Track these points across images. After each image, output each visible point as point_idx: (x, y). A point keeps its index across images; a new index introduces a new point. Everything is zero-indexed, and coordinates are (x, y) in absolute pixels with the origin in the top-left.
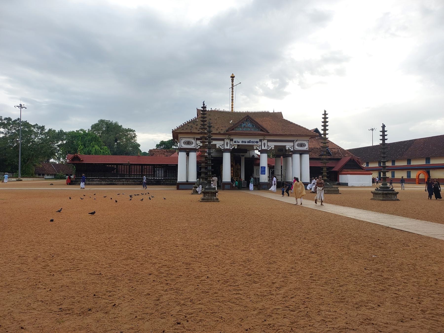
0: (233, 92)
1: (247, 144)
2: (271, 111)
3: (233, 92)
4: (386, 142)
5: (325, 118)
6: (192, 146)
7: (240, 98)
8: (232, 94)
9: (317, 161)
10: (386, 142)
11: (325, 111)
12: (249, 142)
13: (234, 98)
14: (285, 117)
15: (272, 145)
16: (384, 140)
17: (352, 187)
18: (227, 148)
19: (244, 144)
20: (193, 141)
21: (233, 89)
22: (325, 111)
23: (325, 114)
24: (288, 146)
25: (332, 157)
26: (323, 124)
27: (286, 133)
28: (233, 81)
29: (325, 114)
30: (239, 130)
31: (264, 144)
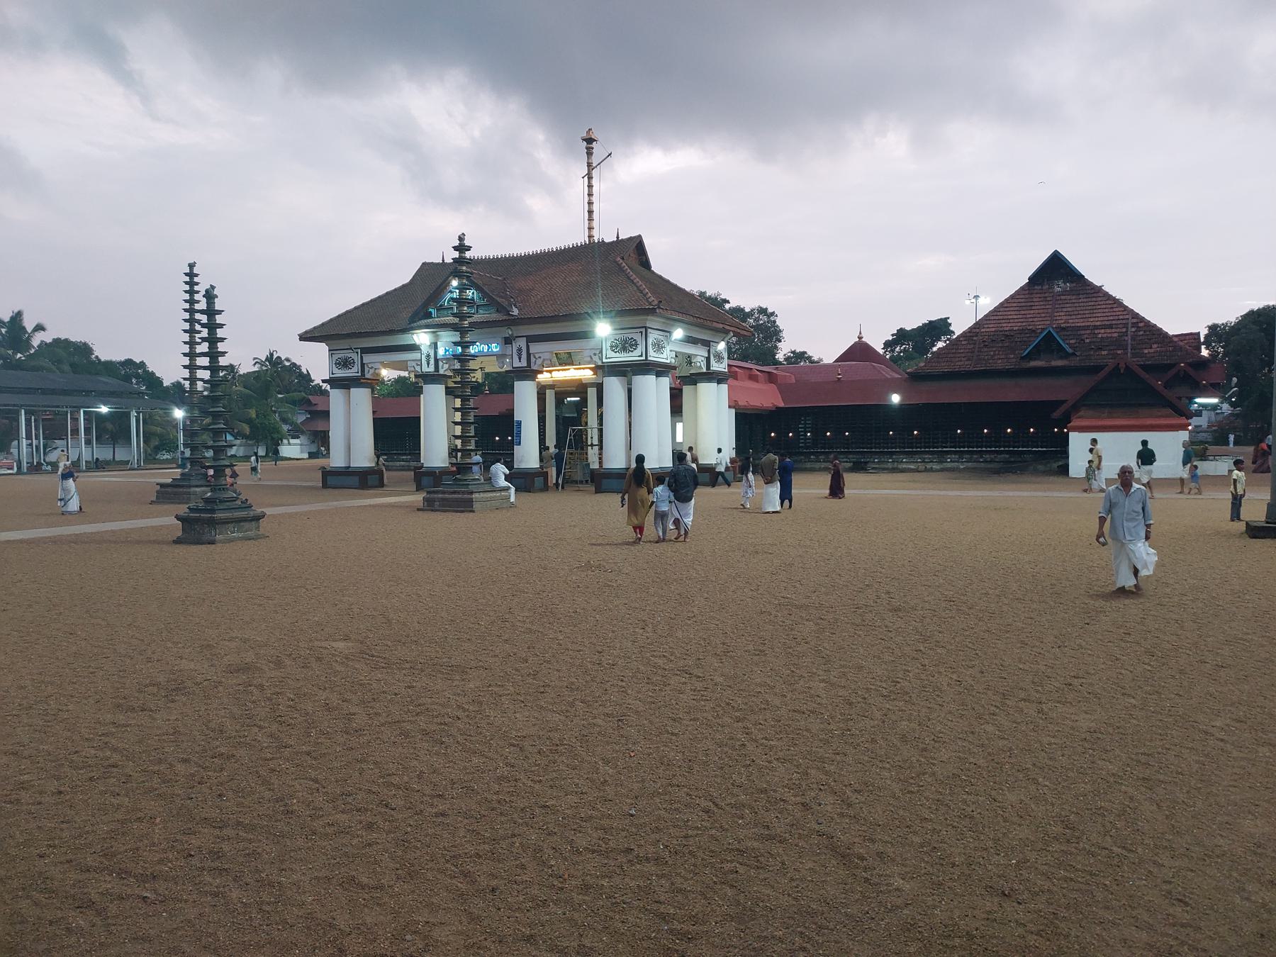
0: (590, 186)
3: (590, 186)
8: (590, 195)
21: (590, 178)
31: (520, 350)
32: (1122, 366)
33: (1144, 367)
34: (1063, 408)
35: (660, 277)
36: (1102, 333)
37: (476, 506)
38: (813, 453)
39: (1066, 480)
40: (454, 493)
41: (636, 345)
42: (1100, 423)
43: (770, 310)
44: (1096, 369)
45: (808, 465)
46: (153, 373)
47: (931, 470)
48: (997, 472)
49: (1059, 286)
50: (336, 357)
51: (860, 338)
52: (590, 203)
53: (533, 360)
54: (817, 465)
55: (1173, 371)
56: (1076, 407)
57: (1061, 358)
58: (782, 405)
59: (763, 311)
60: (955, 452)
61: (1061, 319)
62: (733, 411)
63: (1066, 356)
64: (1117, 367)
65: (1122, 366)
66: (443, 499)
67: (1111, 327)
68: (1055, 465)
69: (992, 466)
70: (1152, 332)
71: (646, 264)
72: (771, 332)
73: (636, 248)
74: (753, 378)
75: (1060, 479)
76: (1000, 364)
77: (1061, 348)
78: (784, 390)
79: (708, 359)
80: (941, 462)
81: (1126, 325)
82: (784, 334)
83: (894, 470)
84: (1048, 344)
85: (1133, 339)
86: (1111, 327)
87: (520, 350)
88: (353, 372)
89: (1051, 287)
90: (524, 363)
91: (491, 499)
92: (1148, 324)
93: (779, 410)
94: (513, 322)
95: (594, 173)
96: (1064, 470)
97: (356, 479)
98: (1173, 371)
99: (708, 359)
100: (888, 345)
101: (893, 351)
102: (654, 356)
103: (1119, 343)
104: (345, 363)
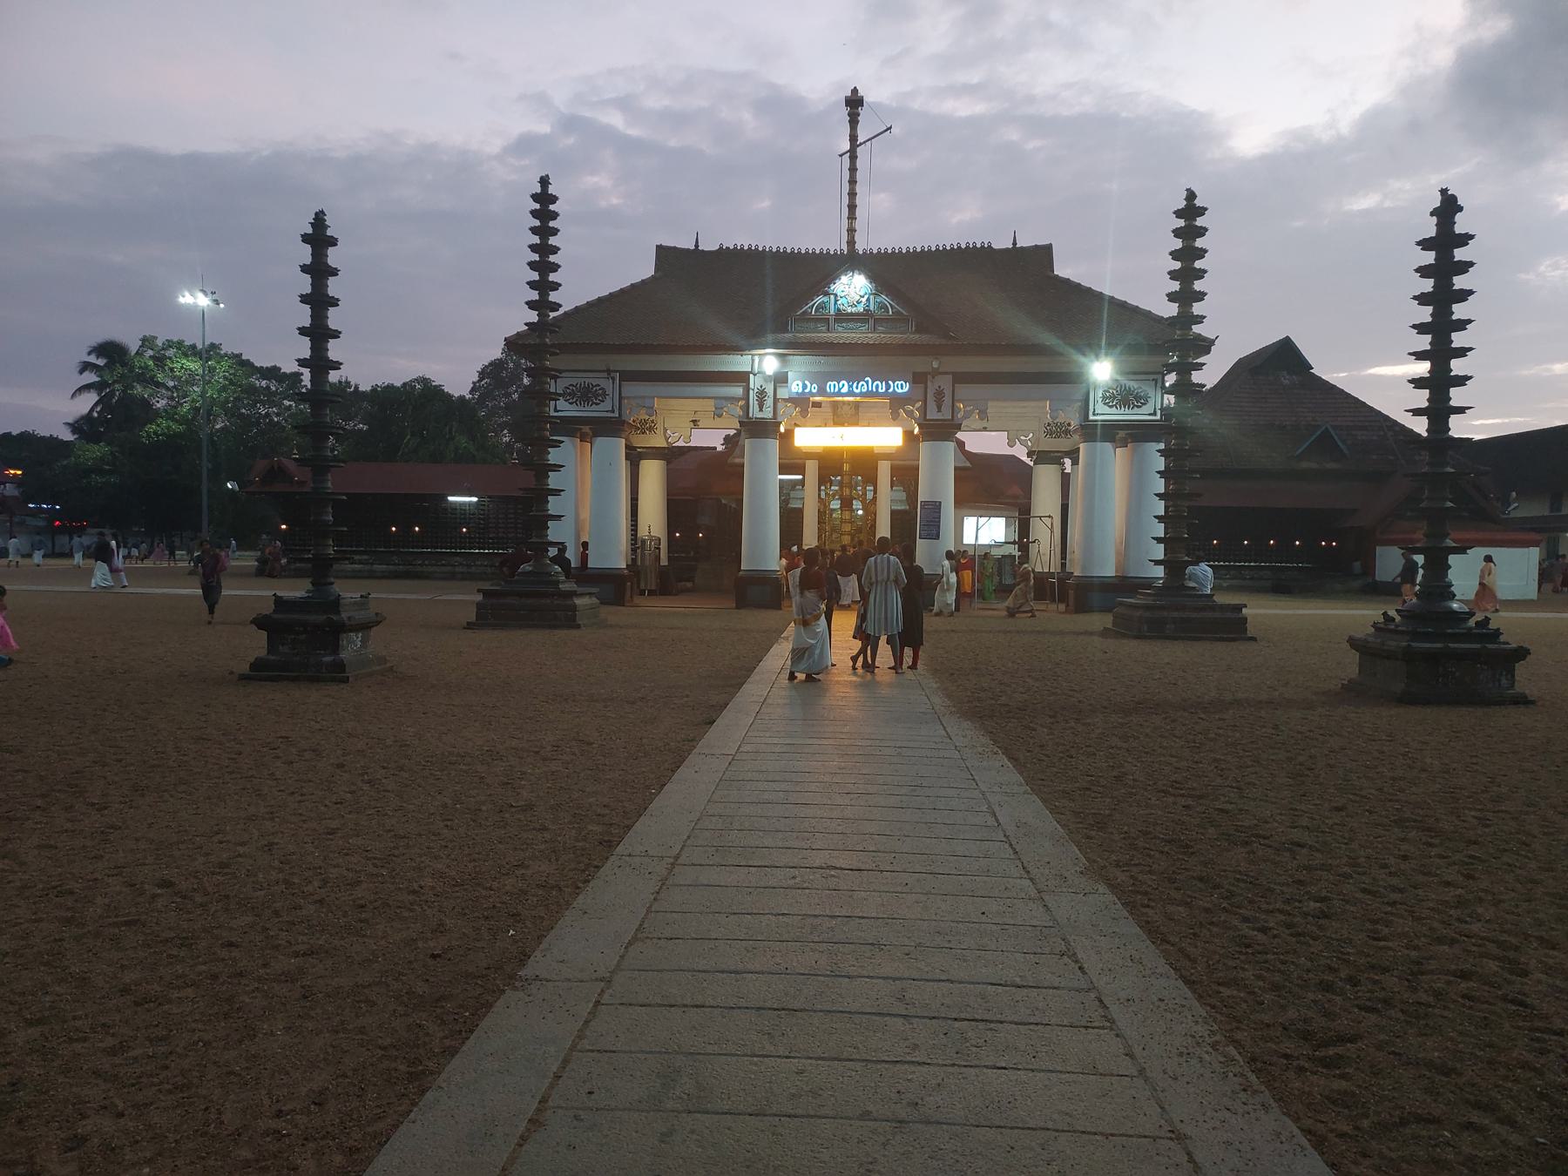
2: (1002, 243)
4: (1459, 428)
6: (602, 407)
7: (873, 202)
10: (1459, 428)
11: (1191, 196)
14: (1063, 269)
16: (544, 286)
18: (760, 415)
20: (606, 384)
21: (853, 158)
22: (1191, 196)
23: (1191, 210)
26: (1175, 286)
28: (854, 121)
29: (1191, 210)
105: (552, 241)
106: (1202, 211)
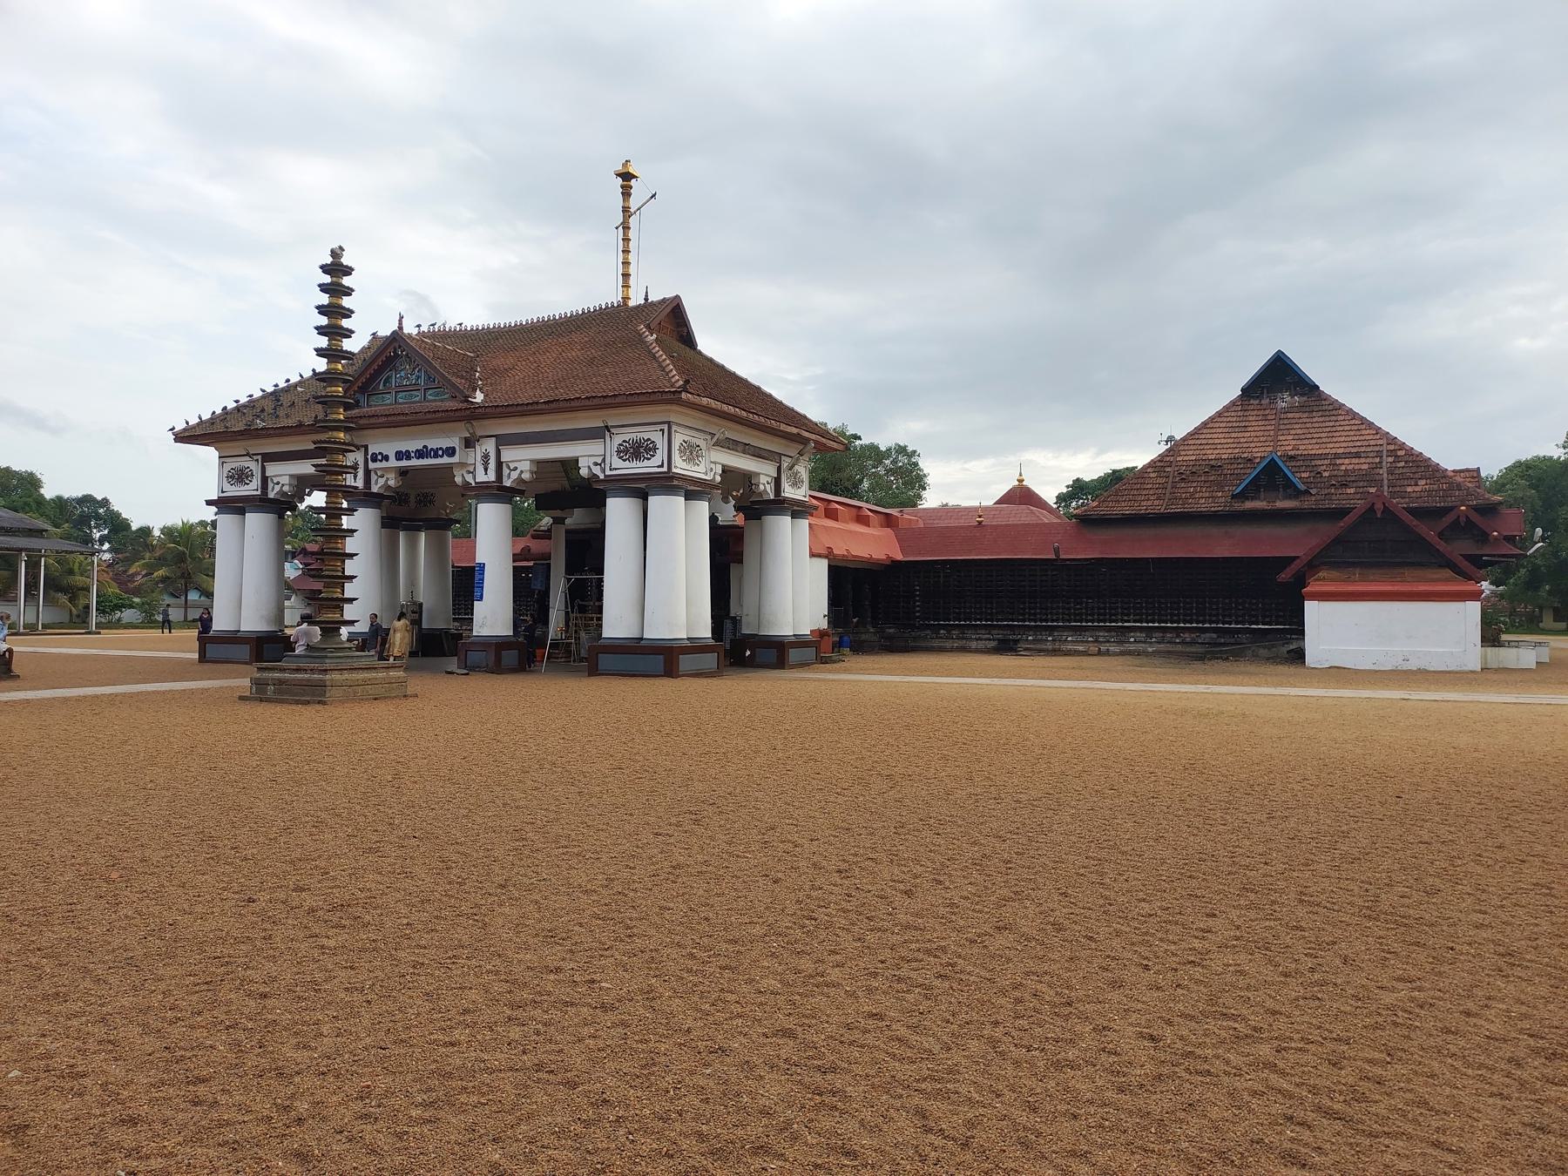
0: (626, 240)
1: (414, 462)
3: (626, 240)
5: (336, 290)
8: (626, 251)
9: (1214, 531)
12: (421, 454)
13: (632, 270)
15: (521, 461)
16: (334, 332)
17: (1338, 674)
19: (404, 463)
21: (626, 228)
23: (336, 268)
24: (590, 457)
25: (1307, 504)
27: (561, 393)
28: (626, 193)
29: (336, 268)
30: (384, 403)
31: (486, 457)
32: (1379, 506)
33: (1411, 511)
34: (1294, 567)
35: (711, 360)
36: (1346, 464)
37: (332, 693)
38: (944, 627)
39: (1300, 670)
40: (298, 670)
41: (655, 449)
42: (1350, 588)
43: (910, 449)
44: (1341, 513)
45: (936, 643)
46: (118, 515)
47: (1107, 653)
48: (1201, 658)
49: (1285, 400)
50: (227, 467)
51: (1021, 481)
52: (626, 263)
53: (506, 471)
54: (948, 644)
55: (1448, 520)
56: (1313, 566)
57: (1290, 497)
58: (900, 557)
59: (902, 450)
60: (1141, 629)
61: (1288, 444)
62: (822, 566)
63: (1298, 494)
64: (1372, 509)
65: (1379, 506)
66: (281, 682)
67: (1357, 455)
68: (1285, 649)
69: (1193, 649)
70: (1419, 465)
71: (688, 340)
72: (913, 480)
73: (673, 319)
74: (862, 519)
75: (1292, 669)
76: (1203, 505)
77: (1289, 484)
78: (906, 537)
79: (778, 481)
80: (1121, 643)
81: (1379, 454)
82: (929, 480)
83: (1055, 652)
84: (1271, 477)
85: (1390, 473)
86: (1357, 455)
87: (486, 457)
88: (252, 488)
89: (1273, 401)
90: (492, 476)
91: (365, 683)
92: (1410, 452)
93: (895, 565)
94: (473, 415)
95: (633, 221)
96: (1298, 656)
97: (244, 651)
98: (1448, 520)
99: (778, 481)
100: (1061, 498)
101: (1067, 506)
102: (681, 466)
103: (1370, 478)
104: (240, 476)
105: (346, 302)
106: (348, 271)
